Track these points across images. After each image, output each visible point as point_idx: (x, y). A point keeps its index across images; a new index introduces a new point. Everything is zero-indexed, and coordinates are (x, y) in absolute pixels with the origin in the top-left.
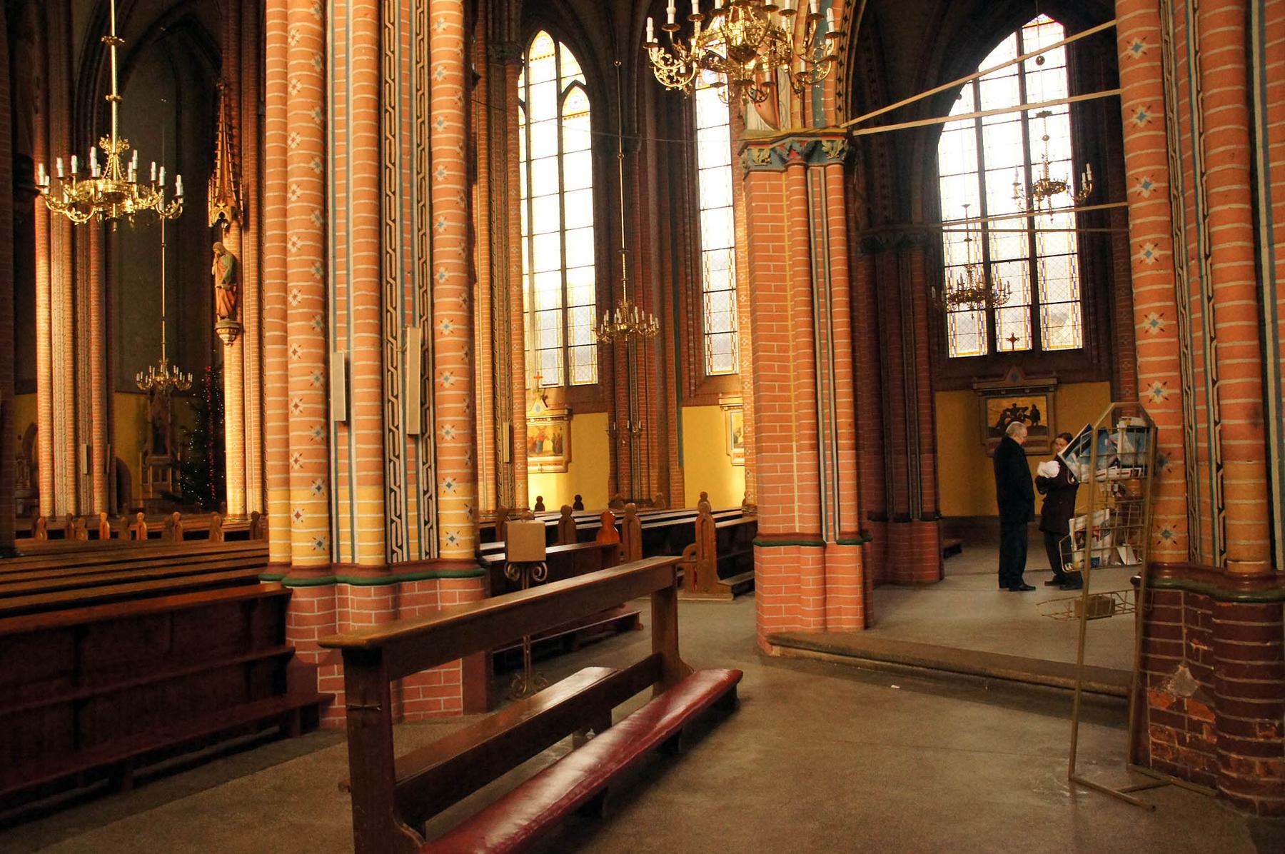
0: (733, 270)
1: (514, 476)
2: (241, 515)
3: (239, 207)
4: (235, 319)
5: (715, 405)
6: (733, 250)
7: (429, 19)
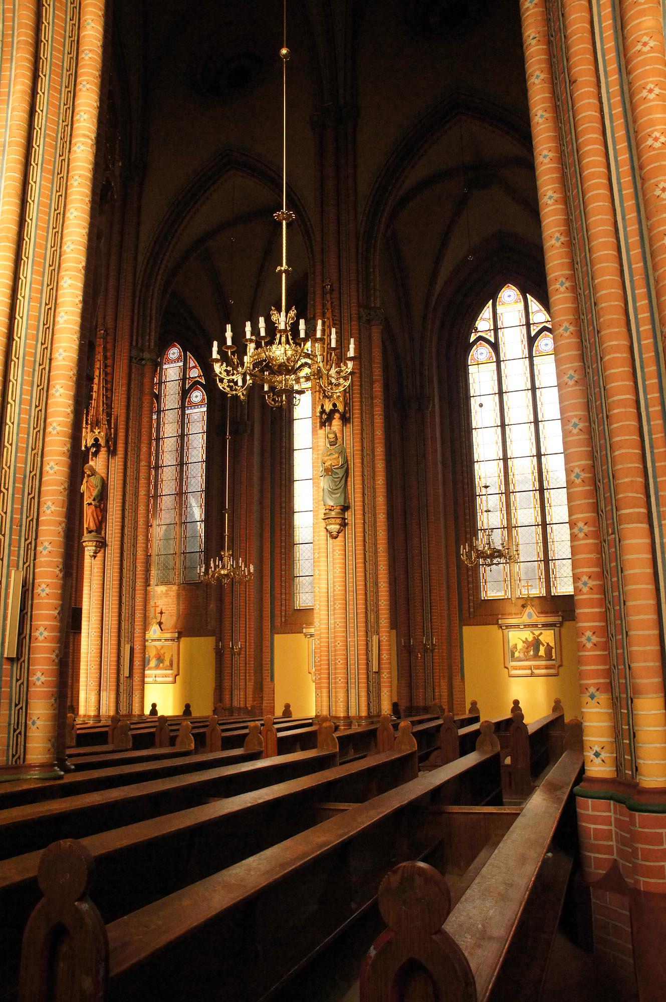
1: (380, 685)
2: (95, 716)
3: (111, 435)
4: (100, 534)
5: (300, 633)
6: (504, 495)
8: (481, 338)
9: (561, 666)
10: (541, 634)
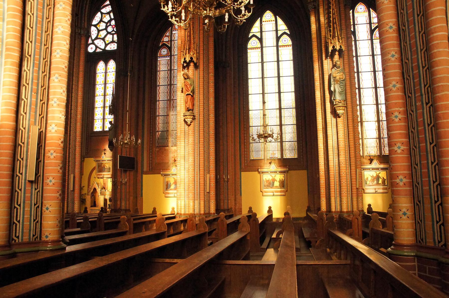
0: (380, 111)
5: (158, 174)
8: (254, 36)
9: (287, 191)
10: (380, 173)
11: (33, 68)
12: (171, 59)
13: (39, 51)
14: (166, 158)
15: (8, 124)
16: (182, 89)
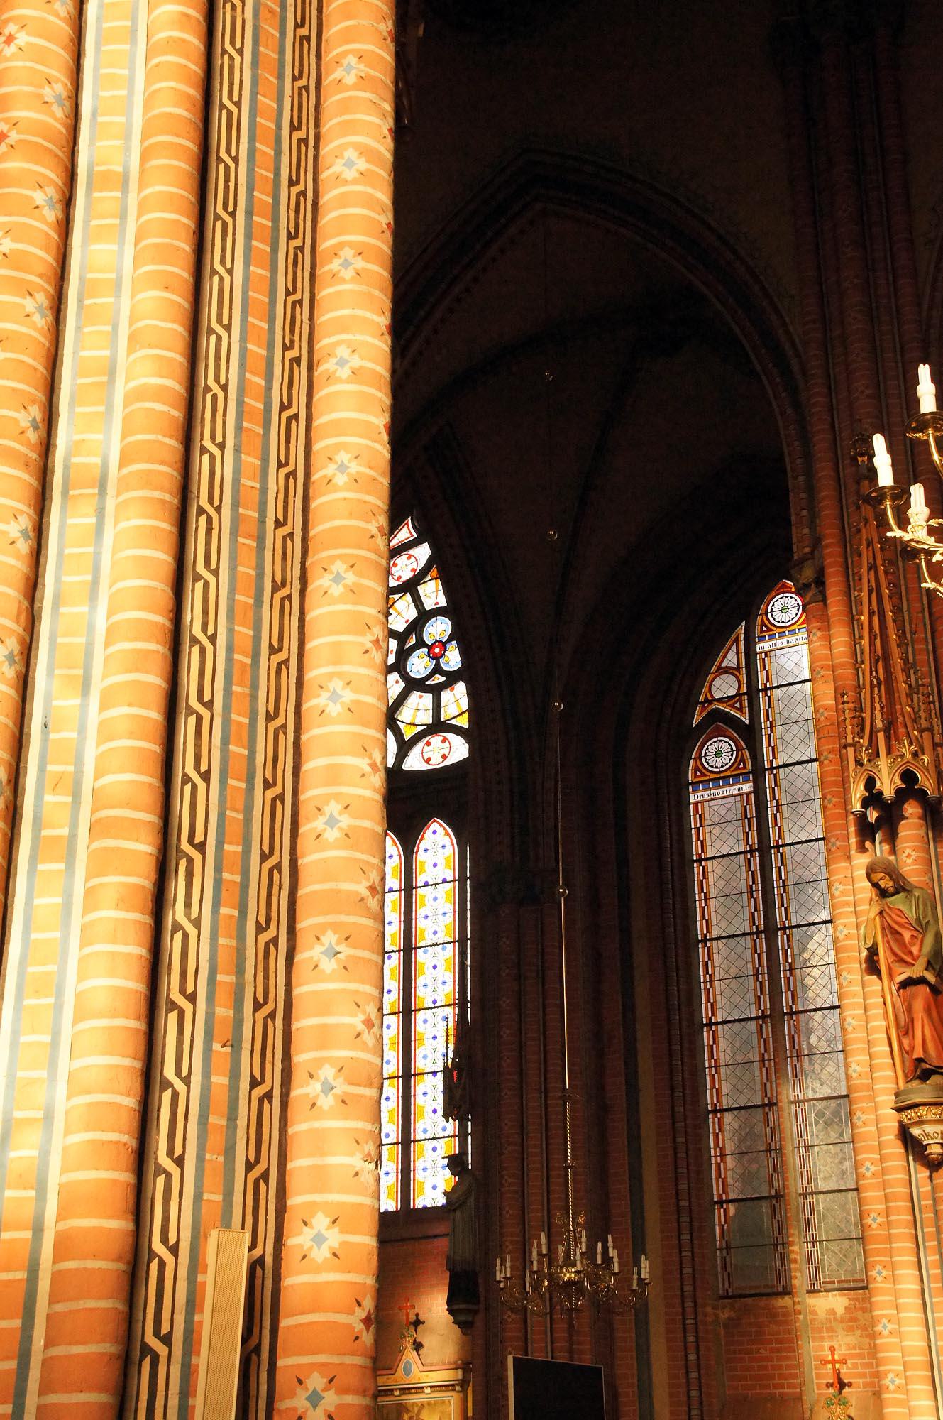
7: (316, 157)
11: (215, 911)
12: (759, 791)
13: (241, 817)
14: (780, 1367)
15: (101, 1229)
16: (873, 951)
